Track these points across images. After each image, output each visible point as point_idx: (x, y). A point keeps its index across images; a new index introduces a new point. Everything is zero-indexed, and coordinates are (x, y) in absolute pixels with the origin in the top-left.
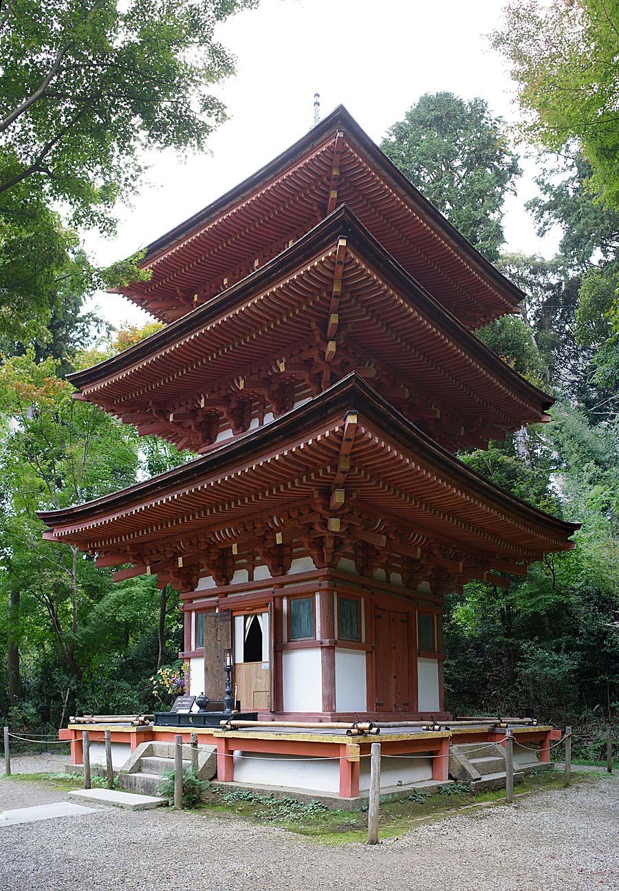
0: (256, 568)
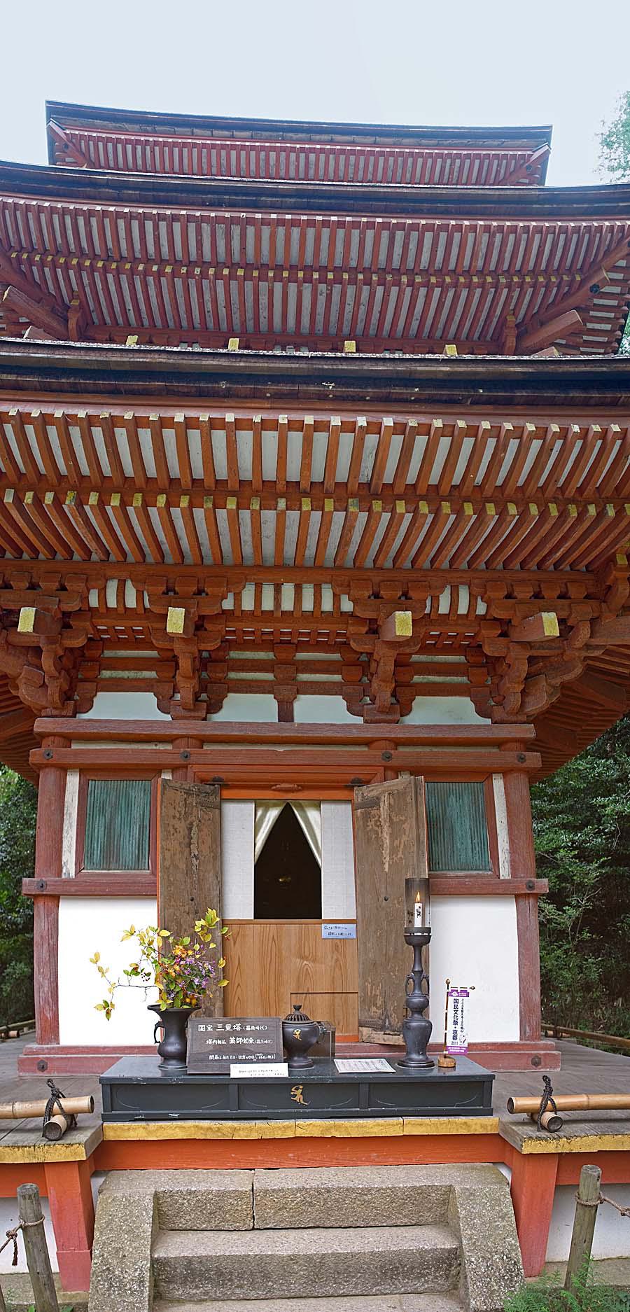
0: (230, 695)
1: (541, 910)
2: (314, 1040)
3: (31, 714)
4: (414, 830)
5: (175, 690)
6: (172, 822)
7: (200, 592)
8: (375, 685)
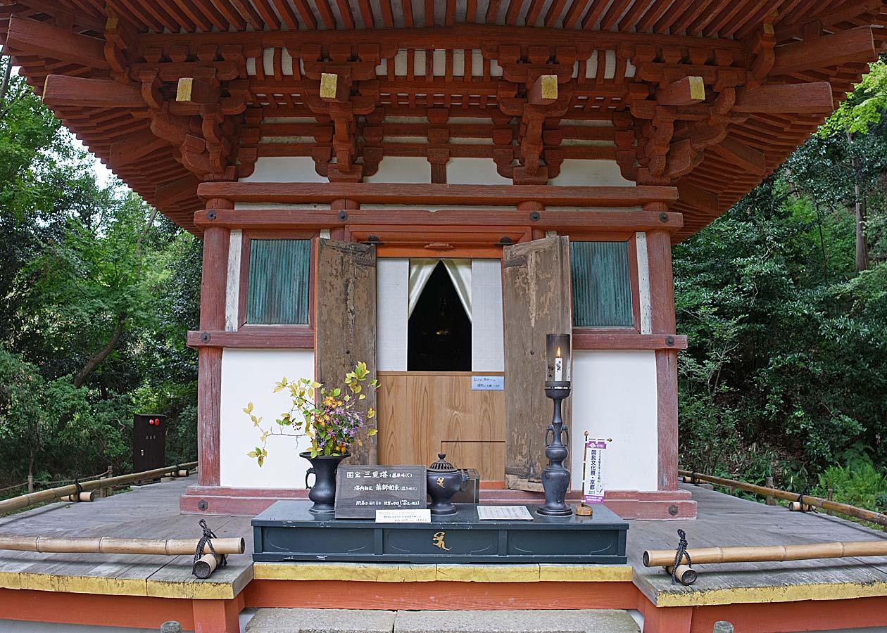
0: (386, 158)
1: (680, 362)
2: (457, 488)
3: (196, 180)
4: (559, 288)
5: (332, 155)
6: (329, 279)
7: (354, 58)
8: (524, 148)
